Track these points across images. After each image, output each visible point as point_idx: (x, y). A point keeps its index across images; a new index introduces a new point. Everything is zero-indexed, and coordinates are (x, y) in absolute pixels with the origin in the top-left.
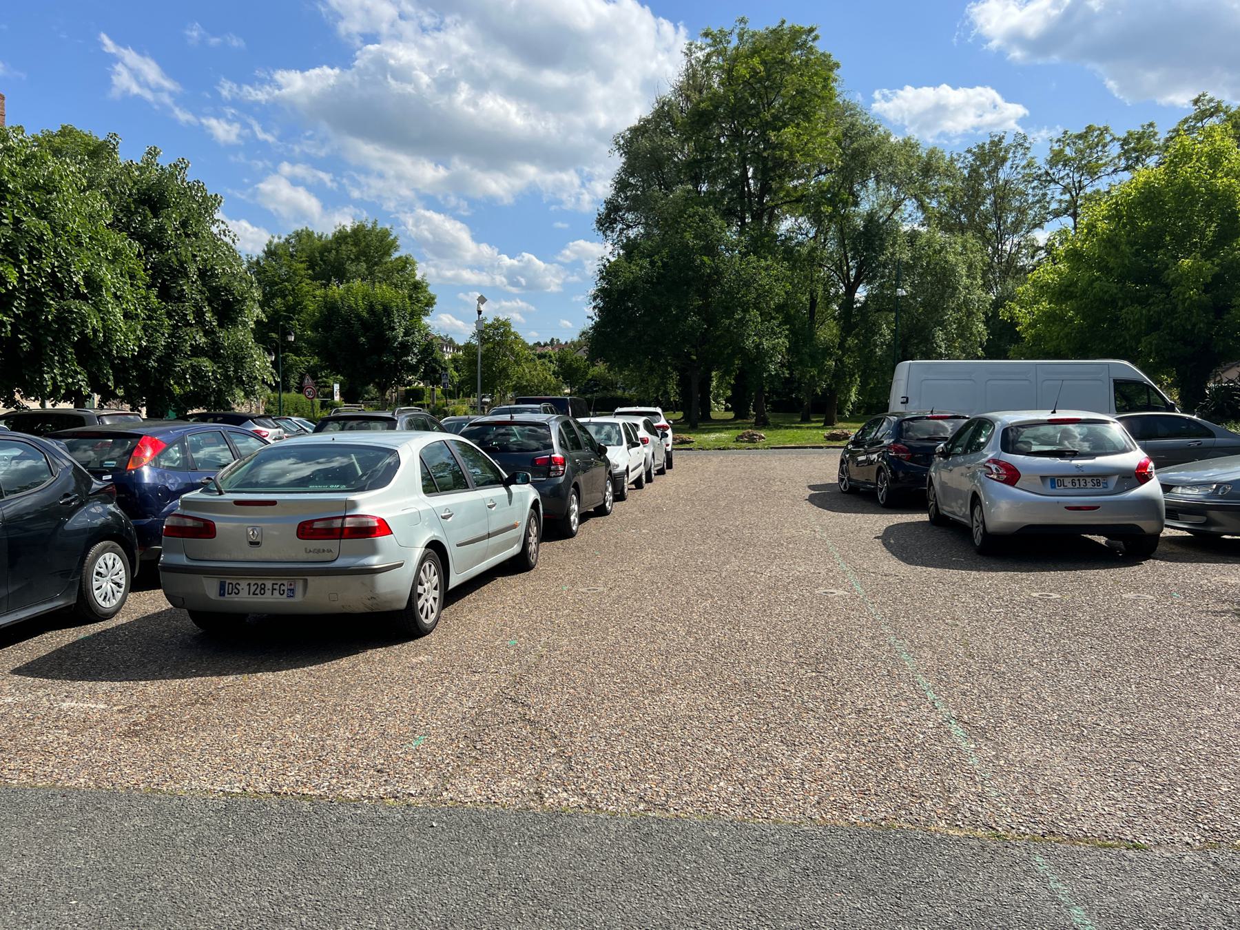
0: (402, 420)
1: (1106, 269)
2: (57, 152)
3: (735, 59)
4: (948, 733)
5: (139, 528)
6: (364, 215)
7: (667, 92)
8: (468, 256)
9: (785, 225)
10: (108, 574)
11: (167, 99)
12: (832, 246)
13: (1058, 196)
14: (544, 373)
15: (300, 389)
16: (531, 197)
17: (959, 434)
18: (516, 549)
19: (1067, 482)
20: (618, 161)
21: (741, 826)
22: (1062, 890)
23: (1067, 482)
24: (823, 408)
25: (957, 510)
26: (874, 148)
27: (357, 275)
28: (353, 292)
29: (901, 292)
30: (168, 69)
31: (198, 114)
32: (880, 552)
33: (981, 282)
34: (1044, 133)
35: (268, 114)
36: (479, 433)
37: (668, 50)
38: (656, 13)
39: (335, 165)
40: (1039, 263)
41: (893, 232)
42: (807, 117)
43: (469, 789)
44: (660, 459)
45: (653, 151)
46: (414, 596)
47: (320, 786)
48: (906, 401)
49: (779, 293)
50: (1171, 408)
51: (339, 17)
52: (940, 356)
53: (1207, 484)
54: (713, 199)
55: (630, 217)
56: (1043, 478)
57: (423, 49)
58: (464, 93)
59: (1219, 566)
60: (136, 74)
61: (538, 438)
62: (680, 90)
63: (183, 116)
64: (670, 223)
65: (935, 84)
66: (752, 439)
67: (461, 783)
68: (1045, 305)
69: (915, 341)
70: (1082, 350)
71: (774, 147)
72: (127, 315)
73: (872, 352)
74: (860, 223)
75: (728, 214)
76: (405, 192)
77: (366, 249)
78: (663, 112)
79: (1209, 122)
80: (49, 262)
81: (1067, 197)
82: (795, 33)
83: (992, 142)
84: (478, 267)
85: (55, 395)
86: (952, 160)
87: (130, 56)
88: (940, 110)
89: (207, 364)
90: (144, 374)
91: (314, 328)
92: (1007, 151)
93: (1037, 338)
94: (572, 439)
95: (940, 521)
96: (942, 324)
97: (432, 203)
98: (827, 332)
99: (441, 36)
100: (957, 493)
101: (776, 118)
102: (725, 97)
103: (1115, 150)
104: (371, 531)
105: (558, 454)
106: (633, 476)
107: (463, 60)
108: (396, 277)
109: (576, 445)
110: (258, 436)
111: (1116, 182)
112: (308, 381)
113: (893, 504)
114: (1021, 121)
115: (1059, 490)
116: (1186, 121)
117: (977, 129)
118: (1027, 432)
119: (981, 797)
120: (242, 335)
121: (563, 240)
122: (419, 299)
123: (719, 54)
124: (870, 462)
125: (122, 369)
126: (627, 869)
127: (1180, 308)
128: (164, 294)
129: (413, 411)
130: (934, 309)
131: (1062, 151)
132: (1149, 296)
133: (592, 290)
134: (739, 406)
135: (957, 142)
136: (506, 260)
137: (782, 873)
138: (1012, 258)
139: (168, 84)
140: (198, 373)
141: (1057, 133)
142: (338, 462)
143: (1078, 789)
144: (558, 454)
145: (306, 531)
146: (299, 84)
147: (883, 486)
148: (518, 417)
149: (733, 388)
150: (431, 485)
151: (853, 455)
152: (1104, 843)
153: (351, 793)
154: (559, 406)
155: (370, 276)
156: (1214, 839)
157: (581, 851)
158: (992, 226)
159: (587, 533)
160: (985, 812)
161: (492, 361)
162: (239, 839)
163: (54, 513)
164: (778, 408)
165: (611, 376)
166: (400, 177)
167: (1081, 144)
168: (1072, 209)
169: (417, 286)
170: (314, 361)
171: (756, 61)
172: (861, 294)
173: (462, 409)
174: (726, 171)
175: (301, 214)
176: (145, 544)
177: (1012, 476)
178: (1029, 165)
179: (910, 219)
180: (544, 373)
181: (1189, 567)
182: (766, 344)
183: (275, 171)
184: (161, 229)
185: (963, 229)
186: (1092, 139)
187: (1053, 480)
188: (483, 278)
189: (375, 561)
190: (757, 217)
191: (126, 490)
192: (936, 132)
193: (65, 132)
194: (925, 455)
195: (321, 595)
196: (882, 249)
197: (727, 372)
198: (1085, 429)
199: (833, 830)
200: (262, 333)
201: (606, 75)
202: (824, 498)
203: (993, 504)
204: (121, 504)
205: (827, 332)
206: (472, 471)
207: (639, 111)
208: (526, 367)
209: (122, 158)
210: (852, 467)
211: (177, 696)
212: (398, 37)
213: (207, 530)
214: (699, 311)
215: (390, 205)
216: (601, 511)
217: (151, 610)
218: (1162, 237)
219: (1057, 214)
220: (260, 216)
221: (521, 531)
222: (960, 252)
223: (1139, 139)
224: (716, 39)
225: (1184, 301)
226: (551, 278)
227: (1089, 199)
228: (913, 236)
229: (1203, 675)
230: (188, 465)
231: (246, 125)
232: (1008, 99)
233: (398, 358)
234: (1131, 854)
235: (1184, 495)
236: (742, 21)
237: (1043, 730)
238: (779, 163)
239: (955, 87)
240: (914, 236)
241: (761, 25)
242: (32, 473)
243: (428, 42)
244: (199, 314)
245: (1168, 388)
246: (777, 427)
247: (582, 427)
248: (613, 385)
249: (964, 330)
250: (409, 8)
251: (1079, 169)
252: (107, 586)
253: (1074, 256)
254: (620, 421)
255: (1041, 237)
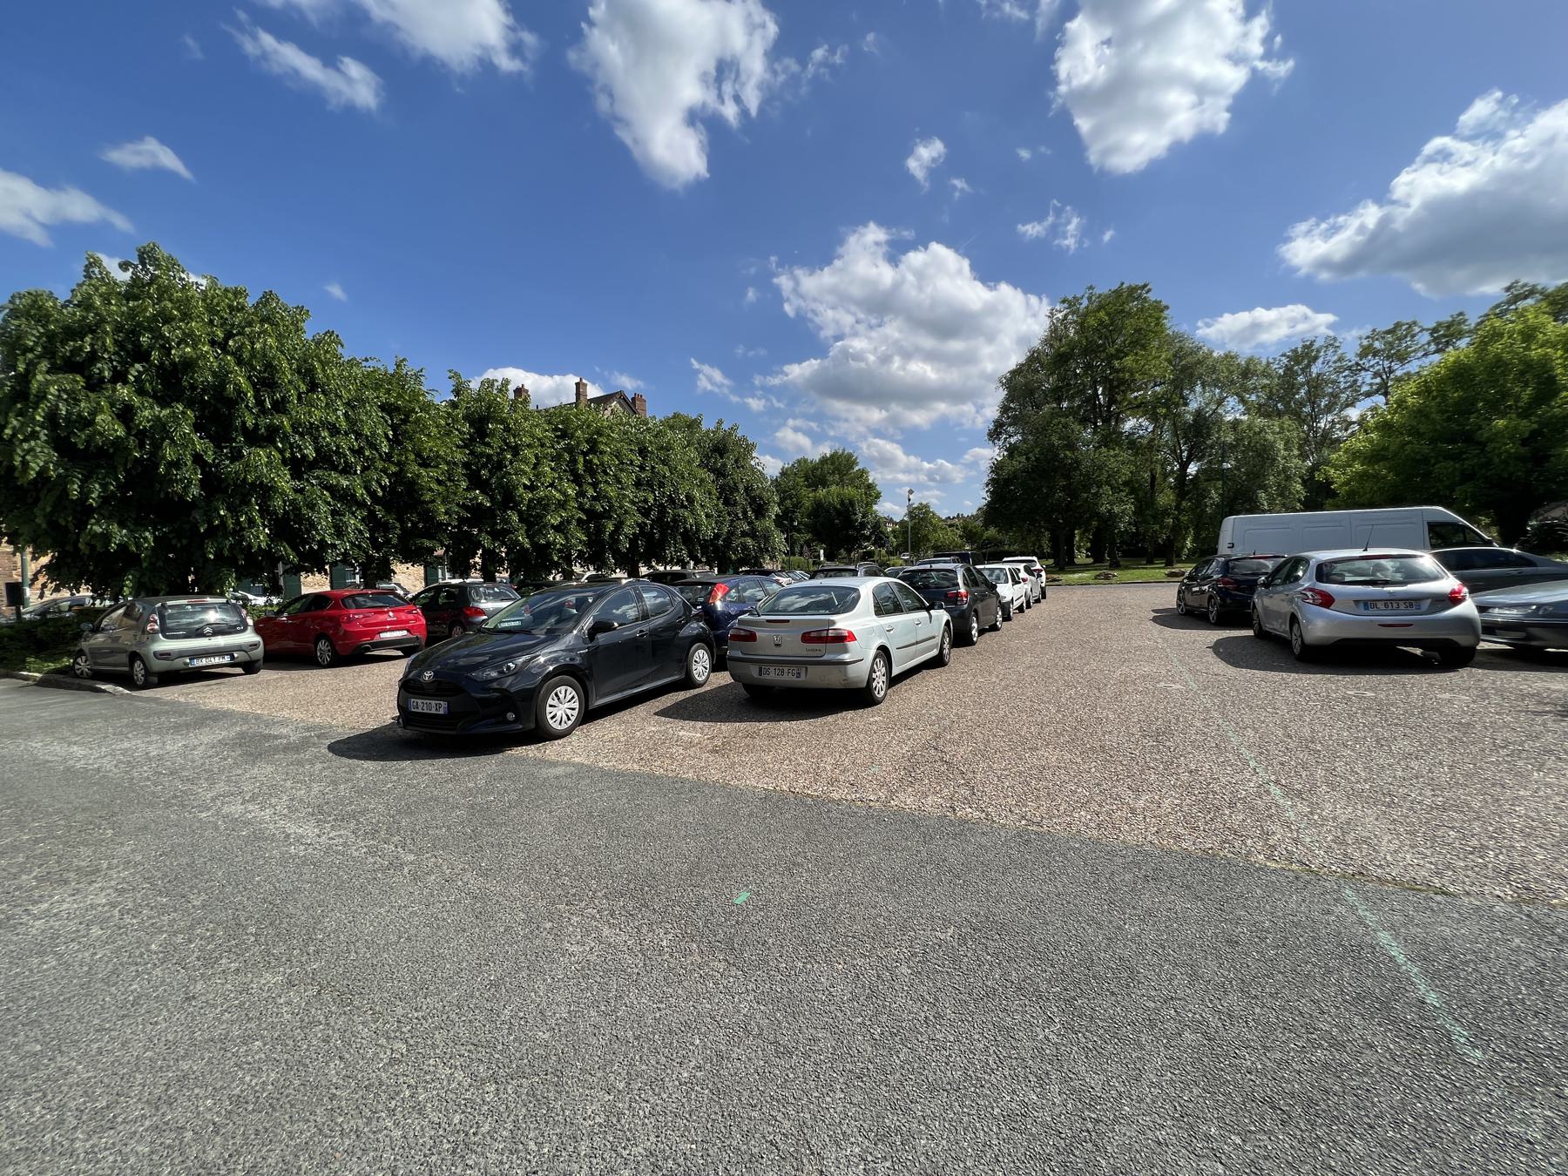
0: (861, 570)
1: (1414, 432)
2: (672, 428)
3: (1086, 315)
4: (1268, 792)
5: (716, 636)
6: (837, 446)
7: (1036, 343)
8: (902, 465)
9: (1129, 424)
10: (700, 661)
11: (726, 391)
12: (1166, 436)
13: (1368, 380)
14: (954, 536)
15: (801, 554)
16: (943, 424)
17: (1278, 570)
18: (935, 652)
19: (1380, 605)
20: (1002, 394)
21: (1097, 842)
22: (1371, 918)
23: (1380, 605)
24: (1165, 553)
25: (1279, 627)
26: (1199, 362)
27: (834, 482)
28: (831, 493)
29: (1227, 466)
30: (726, 374)
31: (742, 396)
32: (1211, 657)
33: (1296, 452)
34: (1355, 333)
35: (781, 392)
36: (910, 577)
37: (1034, 316)
38: (1026, 292)
39: (820, 417)
40: (1353, 434)
41: (1219, 421)
42: (1144, 347)
43: (907, 800)
44: (1037, 592)
45: (1026, 385)
46: (871, 680)
47: (818, 790)
48: (1232, 546)
49: (1126, 472)
50: (1489, 543)
51: (820, 328)
52: (1264, 512)
53: (1529, 605)
54: (1072, 411)
55: (1011, 429)
56: (1357, 602)
57: (870, 339)
58: (897, 362)
59: (1542, 675)
60: (710, 379)
61: (948, 579)
62: (1046, 342)
63: (734, 399)
64: (1041, 431)
65: (1250, 308)
66: (1107, 577)
67: (902, 796)
68: (1358, 467)
69: (1241, 500)
70: (1396, 500)
71: (1117, 371)
72: (707, 516)
73: (1203, 511)
74: (1190, 418)
75: (1084, 421)
76: (861, 429)
77: (840, 466)
78: (1034, 358)
79: (1521, 304)
80: (668, 490)
81: (1378, 380)
82: (1132, 290)
83: (1305, 347)
84: (907, 471)
85: (671, 562)
86: (1268, 364)
87: (706, 368)
88: (1256, 327)
89: (749, 541)
90: (716, 548)
91: (809, 517)
92: (1318, 351)
93: (1351, 494)
94: (973, 580)
95: (1262, 635)
96: (1264, 488)
97: (878, 434)
98: (1165, 498)
99: (881, 330)
100: (1278, 615)
101: (1118, 351)
102: (1079, 342)
103: (1426, 337)
104: (842, 639)
105: (962, 590)
106: (1016, 604)
107: (896, 342)
108: (857, 482)
109: (975, 583)
110: (777, 582)
111: (1425, 363)
112: (805, 548)
113: (1221, 624)
114: (1331, 326)
115: (1414, 610)
116: (1498, 306)
117: (1289, 337)
118: (1339, 567)
119: (1296, 841)
120: (769, 523)
121: (964, 449)
122: (872, 494)
123: (1073, 313)
124: (1203, 592)
125: (705, 546)
126: (1012, 861)
127: (1496, 460)
128: (726, 503)
129: (868, 564)
130: (1256, 477)
131: (1371, 345)
132: (1462, 453)
133: (986, 480)
134: (1097, 554)
135: (1272, 349)
136: (926, 465)
137: (1128, 877)
138: (1326, 434)
139: (726, 382)
140: (745, 547)
141: (1367, 331)
142: (823, 597)
143: (1386, 845)
144: (962, 590)
145: (806, 638)
146: (797, 371)
147: (1214, 610)
148: (934, 566)
149: (1091, 541)
150: (880, 610)
151: (1189, 587)
152: (1413, 887)
153: (835, 796)
154: (963, 558)
155: (841, 483)
156: (1527, 897)
157: (981, 846)
158: (1307, 409)
159: (984, 643)
160: (1299, 851)
161: (918, 531)
162: (773, 816)
163: (673, 627)
164: (1126, 554)
165: (1000, 537)
166: (858, 420)
167: (1389, 338)
168: (1384, 390)
169: (870, 487)
170: (808, 536)
171: (1102, 314)
172: (1192, 469)
173: (903, 562)
174: (1083, 392)
175: (800, 448)
176: (719, 646)
177: (1327, 601)
178: (1340, 359)
179: (1232, 411)
180: (954, 536)
181: (1509, 674)
182: (1116, 510)
183: (785, 425)
184: (724, 465)
185: (1280, 414)
186: (1402, 332)
187: (1367, 604)
188: (912, 478)
189: (846, 657)
190: (1106, 421)
191: (709, 614)
192: (1253, 344)
193: (676, 416)
194: (1251, 586)
195: (815, 677)
196: (1209, 435)
197: (1087, 530)
198: (1397, 563)
199: (1170, 852)
200: (779, 521)
201: (991, 338)
202: (1165, 618)
203: (1309, 622)
204: (707, 622)
205: (1165, 498)
206: (906, 602)
207: (1015, 359)
208: (940, 534)
209: (704, 428)
210: (1188, 596)
211: (738, 731)
212: (855, 334)
213: (751, 637)
214: (1064, 489)
215: (852, 438)
216: (994, 628)
217: (723, 683)
218: (1474, 404)
219: (1368, 395)
220: (776, 452)
221: (938, 640)
222: (1278, 433)
223: (1448, 327)
224: (1071, 304)
225: (1499, 456)
226: (956, 473)
227: (1398, 380)
228: (1235, 424)
229: (1520, 763)
230: (741, 600)
231: (768, 400)
232: (1317, 310)
233: (859, 531)
234: (1439, 898)
235: (1499, 615)
236: (1091, 288)
237: (1353, 796)
238: (1122, 382)
239: (1268, 308)
240: (1236, 423)
241: (1104, 288)
242: (663, 605)
243: (874, 334)
244: (745, 513)
245: (1486, 528)
246: (1127, 568)
247: (979, 571)
248: (1002, 543)
249: (1283, 491)
250: (862, 316)
251: (1388, 357)
252: (700, 668)
253: (1385, 427)
254: (1007, 567)
255: (1353, 414)
